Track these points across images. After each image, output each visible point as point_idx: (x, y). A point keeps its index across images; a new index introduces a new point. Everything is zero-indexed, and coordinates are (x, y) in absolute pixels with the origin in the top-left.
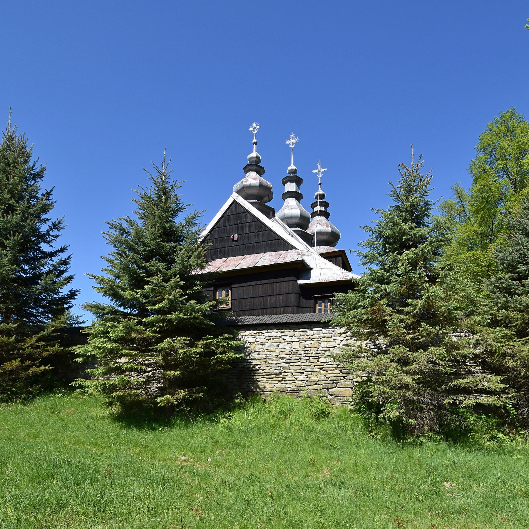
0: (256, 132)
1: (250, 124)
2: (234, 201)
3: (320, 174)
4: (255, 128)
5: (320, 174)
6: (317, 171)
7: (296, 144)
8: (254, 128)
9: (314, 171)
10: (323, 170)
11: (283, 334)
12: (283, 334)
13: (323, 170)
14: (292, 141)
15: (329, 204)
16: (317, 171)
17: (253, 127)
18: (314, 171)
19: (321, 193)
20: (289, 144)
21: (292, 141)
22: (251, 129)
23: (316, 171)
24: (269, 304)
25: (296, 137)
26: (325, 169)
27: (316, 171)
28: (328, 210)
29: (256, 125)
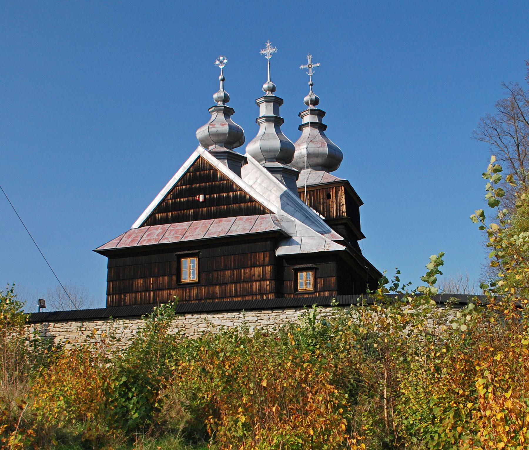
0: (223, 67)
1: (217, 58)
2: (199, 157)
3: (310, 70)
4: (221, 62)
5: (310, 70)
6: (310, 62)
7: (274, 54)
8: (222, 62)
9: (302, 67)
10: (315, 65)
11: (259, 318)
12: (259, 318)
13: (315, 65)
14: (269, 51)
15: (325, 113)
16: (310, 62)
17: (219, 60)
18: (302, 67)
19: (314, 97)
20: (265, 55)
21: (269, 51)
22: (217, 62)
23: (305, 67)
24: (242, 277)
25: (273, 46)
26: (318, 65)
27: (305, 67)
28: (324, 121)
29: (224, 59)
